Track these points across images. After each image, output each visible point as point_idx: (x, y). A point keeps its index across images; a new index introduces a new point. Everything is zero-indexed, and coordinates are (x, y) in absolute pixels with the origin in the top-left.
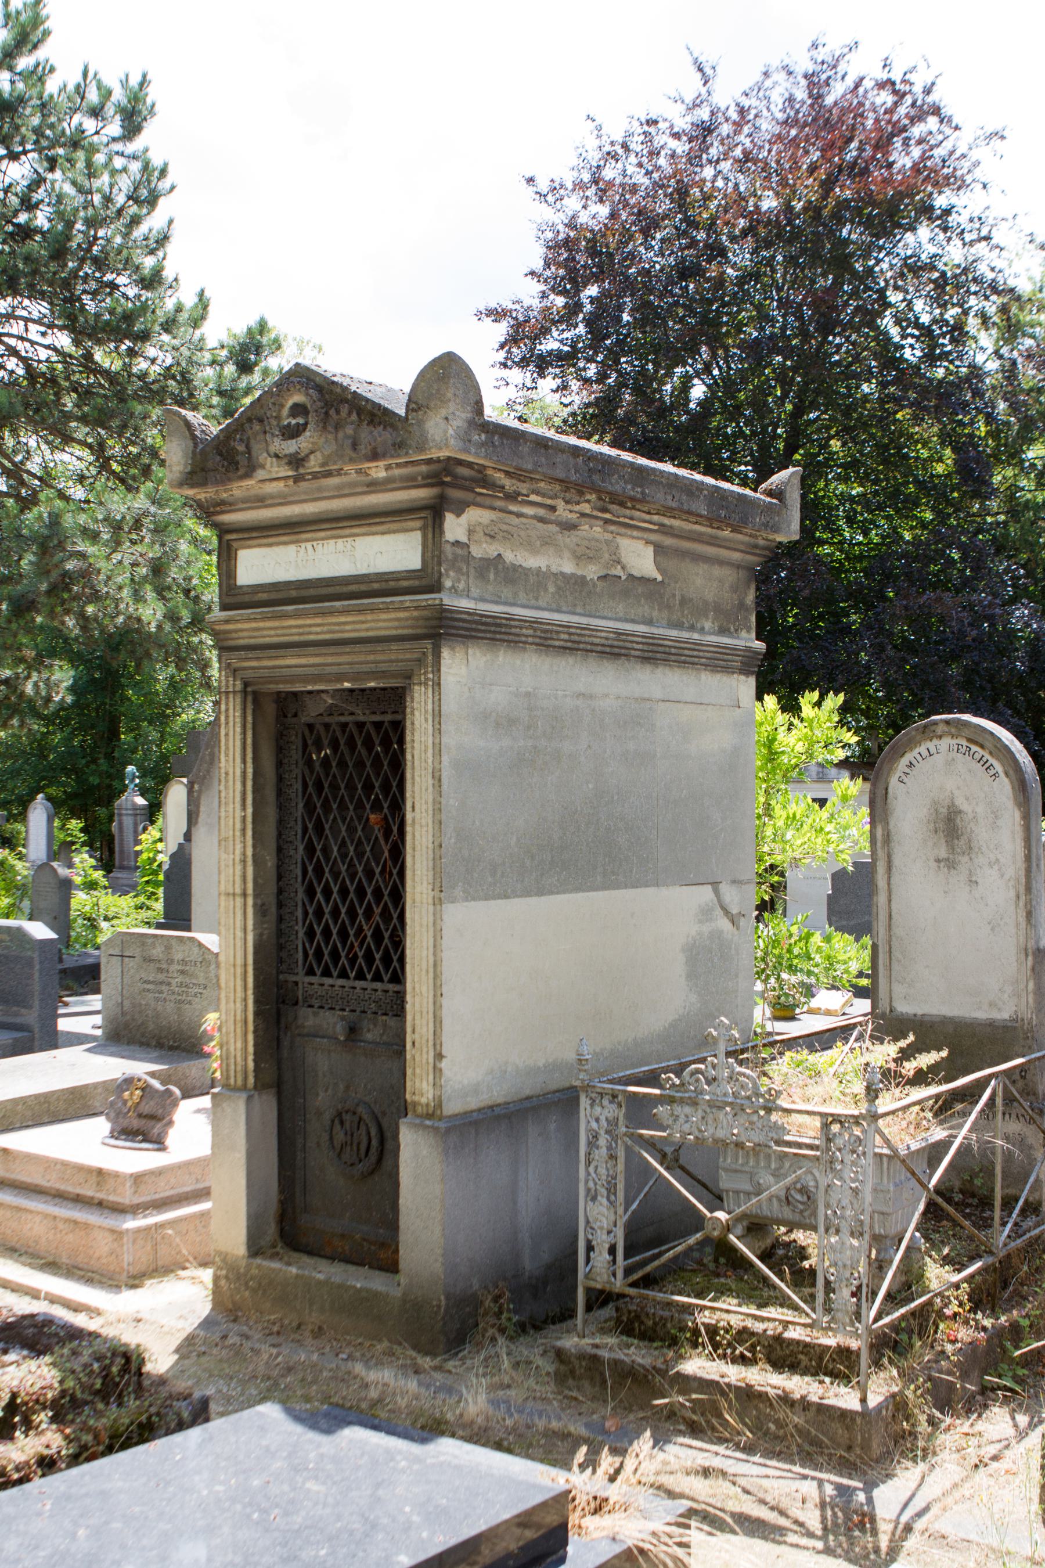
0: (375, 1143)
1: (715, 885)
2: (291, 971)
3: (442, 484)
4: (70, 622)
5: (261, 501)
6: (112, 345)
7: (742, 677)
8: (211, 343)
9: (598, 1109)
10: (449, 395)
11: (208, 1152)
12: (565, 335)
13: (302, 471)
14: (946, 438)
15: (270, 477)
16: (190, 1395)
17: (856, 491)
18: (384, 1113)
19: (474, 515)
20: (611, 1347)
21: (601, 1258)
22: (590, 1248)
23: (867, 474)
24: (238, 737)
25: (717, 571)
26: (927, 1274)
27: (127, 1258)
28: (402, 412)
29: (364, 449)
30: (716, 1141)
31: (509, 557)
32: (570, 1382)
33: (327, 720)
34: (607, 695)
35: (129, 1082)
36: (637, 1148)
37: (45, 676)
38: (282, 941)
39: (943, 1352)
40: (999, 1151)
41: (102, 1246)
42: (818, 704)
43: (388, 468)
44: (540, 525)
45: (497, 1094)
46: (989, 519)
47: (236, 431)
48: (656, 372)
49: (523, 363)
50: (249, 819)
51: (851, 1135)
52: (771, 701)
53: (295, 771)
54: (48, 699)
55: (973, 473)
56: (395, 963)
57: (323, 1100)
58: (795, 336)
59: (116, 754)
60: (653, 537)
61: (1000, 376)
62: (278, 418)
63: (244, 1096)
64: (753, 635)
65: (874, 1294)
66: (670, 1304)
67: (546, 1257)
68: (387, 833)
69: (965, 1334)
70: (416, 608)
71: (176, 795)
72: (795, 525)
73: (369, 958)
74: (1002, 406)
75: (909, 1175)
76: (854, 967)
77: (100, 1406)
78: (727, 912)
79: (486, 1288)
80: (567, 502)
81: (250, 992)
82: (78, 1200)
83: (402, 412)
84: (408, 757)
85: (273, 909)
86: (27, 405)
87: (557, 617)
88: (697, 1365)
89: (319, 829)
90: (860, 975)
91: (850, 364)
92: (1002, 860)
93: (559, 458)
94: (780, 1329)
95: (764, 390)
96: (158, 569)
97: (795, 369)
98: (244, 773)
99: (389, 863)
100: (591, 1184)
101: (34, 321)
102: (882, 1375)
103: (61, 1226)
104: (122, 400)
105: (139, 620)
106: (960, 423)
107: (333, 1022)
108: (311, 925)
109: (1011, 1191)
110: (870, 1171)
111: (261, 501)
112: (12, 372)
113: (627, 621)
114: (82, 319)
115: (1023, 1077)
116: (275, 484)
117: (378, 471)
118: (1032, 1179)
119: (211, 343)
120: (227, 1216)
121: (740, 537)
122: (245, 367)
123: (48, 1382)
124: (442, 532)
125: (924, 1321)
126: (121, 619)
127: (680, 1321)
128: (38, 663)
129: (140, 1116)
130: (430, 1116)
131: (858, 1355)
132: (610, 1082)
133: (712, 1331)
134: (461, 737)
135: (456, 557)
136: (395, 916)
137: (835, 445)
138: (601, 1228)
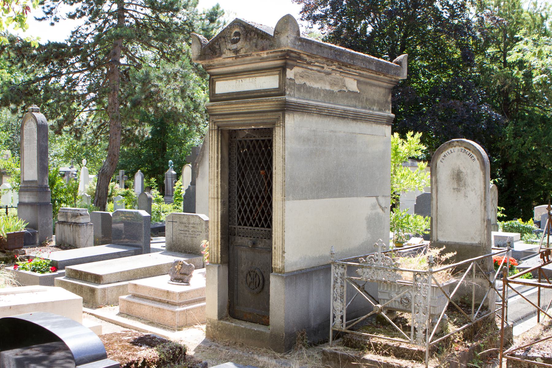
0: (261, 282)
1: (377, 197)
2: (233, 224)
3: (286, 59)
4: (151, 109)
5: (224, 65)
6: (166, 13)
7: (387, 126)
8: (200, 12)
9: (337, 270)
10: (289, 29)
11: (205, 286)
12: (323, 9)
13: (238, 55)
14: (458, 45)
15: (227, 57)
16: (201, 362)
17: (426, 64)
18: (264, 272)
19: (296, 69)
20: (341, 350)
21: (338, 320)
22: (334, 317)
23: (429, 57)
24: (216, 145)
25: (378, 90)
26: (449, 328)
27: (177, 320)
28: (272, 34)
29: (259, 47)
30: (377, 281)
31: (308, 84)
32: (327, 362)
33: (246, 139)
34: (341, 131)
35: (176, 262)
36: (351, 283)
37: (142, 128)
38: (230, 214)
39: (454, 354)
40: (474, 286)
41: (168, 317)
42: (413, 136)
43: (267, 53)
44: (318, 73)
45: (303, 265)
46: (473, 74)
47: (215, 41)
48: (355, 22)
49: (308, 18)
50: (219, 172)
51: (424, 278)
52: (396, 135)
53: (235, 156)
54: (143, 136)
55: (468, 57)
56: (269, 221)
57: (244, 267)
58: (404, 9)
59: (165, 156)
60: (357, 78)
61: (477, 23)
62: (230, 37)
63: (217, 266)
64: (391, 112)
65: (431, 334)
66: (361, 336)
67: (319, 321)
68: (266, 177)
69: (461, 348)
70: (277, 101)
71: (187, 170)
72: (405, 74)
73: (260, 219)
74: (478, 34)
75: (443, 294)
76: (424, 227)
77: (172, 364)
78: (381, 207)
79: (298, 331)
80: (328, 65)
81: (219, 231)
82: (160, 301)
83: (272, 34)
84: (274, 151)
85: (227, 203)
86: (136, 34)
87: (324, 104)
88: (370, 356)
89: (243, 176)
90: (426, 230)
91: (424, 19)
92: (476, 189)
93: (326, 50)
94: (398, 344)
95: (393, 28)
96: (183, 91)
97: (404, 21)
98: (218, 157)
99: (267, 187)
100: (335, 295)
101: (139, 5)
102: (433, 360)
103: (154, 310)
104: (169, 32)
105: (176, 108)
106: (463, 40)
107: (247, 241)
108: (240, 209)
109: (478, 302)
110: (430, 291)
111: (224, 65)
112: (131, 23)
113: (347, 106)
114: (156, 4)
115: (483, 263)
116: (229, 59)
117: (264, 55)
118: (485, 297)
119: (200, 12)
120: (211, 307)
121: (386, 78)
122: (212, 21)
123: (156, 355)
124: (286, 75)
125: (447, 343)
126: (170, 108)
127: (364, 341)
128: (141, 123)
129: (181, 274)
130: (280, 272)
131: (425, 353)
132: (341, 261)
133: (375, 345)
134: (292, 145)
135: (290, 83)
136: (269, 205)
137: (418, 48)
138: (338, 310)
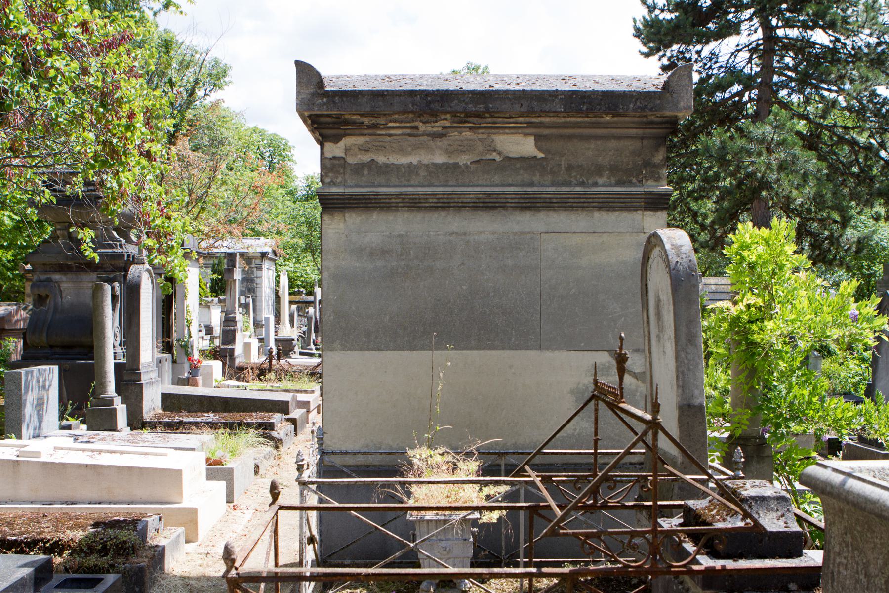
52: (763, 229)
80: (424, 123)
